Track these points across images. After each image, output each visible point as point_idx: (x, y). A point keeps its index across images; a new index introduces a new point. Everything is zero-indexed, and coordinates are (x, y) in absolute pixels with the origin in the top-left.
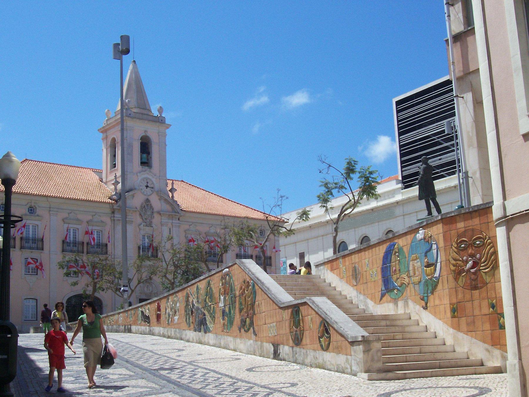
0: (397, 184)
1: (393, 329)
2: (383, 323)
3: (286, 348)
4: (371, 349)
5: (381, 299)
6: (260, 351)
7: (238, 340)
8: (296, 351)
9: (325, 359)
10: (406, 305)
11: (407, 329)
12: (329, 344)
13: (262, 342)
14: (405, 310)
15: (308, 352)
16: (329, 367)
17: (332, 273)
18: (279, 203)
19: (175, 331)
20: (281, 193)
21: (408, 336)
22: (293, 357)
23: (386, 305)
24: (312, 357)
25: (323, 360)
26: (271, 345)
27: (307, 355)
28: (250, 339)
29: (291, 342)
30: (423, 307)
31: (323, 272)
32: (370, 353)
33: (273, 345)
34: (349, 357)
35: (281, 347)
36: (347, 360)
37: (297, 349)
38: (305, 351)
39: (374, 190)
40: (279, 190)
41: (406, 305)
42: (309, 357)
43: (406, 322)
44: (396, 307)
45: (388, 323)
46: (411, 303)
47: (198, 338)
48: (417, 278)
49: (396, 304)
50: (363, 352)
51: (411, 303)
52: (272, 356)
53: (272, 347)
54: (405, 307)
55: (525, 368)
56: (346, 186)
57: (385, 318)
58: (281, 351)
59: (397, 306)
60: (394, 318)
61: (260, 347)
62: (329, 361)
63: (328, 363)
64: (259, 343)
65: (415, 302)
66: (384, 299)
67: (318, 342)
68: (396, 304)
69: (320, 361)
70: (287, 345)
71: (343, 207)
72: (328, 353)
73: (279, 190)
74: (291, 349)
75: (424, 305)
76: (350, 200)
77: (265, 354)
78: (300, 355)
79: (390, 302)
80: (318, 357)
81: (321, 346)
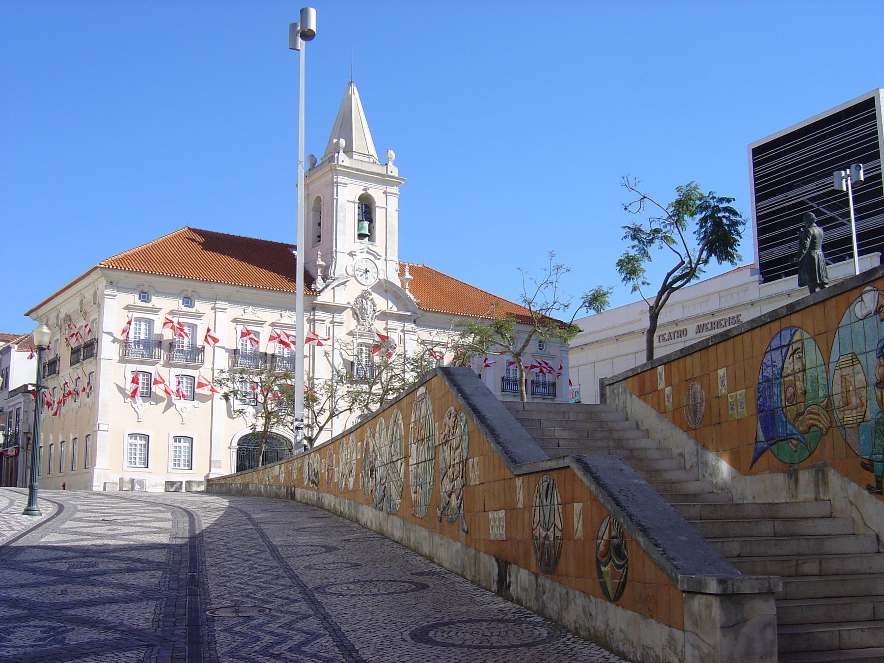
0: (752, 275)
1: (792, 546)
2: (766, 528)
3: (524, 574)
4: (746, 621)
5: (755, 460)
6: (473, 569)
7: (437, 538)
8: (544, 586)
9: (611, 626)
10: (821, 479)
11: (830, 546)
12: (623, 585)
13: (477, 551)
14: (817, 492)
15: (571, 596)
16: (621, 648)
17: (642, 402)
18: (553, 278)
19: (350, 504)
20: (556, 261)
21: (834, 565)
22: (537, 598)
23: (767, 476)
24: (580, 609)
25: (608, 625)
26: (493, 559)
27: (568, 603)
28: (456, 539)
29: (533, 563)
30: (869, 488)
31: (622, 398)
32: (746, 629)
33: (497, 560)
34: (678, 634)
35: (513, 568)
36: (671, 640)
37: (546, 582)
38: (564, 591)
39: (732, 248)
40: (552, 255)
41: (821, 479)
42: (572, 606)
43: (823, 527)
44: (792, 485)
45: (779, 526)
46: (834, 478)
47: (378, 523)
48: (854, 413)
49: (793, 474)
50: (722, 627)
51: (834, 478)
52: (494, 587)
53: (495, 564)
54: (817, 485)
55: (198, 228)
56: (676, 236)
57: (770, 512)
58: (513, 579)
59: (796, 481)
60: (791, 512)
61: (473, 561)
62: (621, 630)
63: (618, 636)
64: (473, 551)
65: (844, 473)
66: (763, 460)
67: (595, 575)
68: (793, 474)
69: (599, 624)
70: (527, 567)
71: (669, 275)
72: (620, 609)
73: (552, 255)
74: (533, 578)
75: (873, 484)
76: (683, 262)
77: (482, 578)
78: (552, 598)
79: (778, 471)
80: (593, 613)
81: (604, 586)
